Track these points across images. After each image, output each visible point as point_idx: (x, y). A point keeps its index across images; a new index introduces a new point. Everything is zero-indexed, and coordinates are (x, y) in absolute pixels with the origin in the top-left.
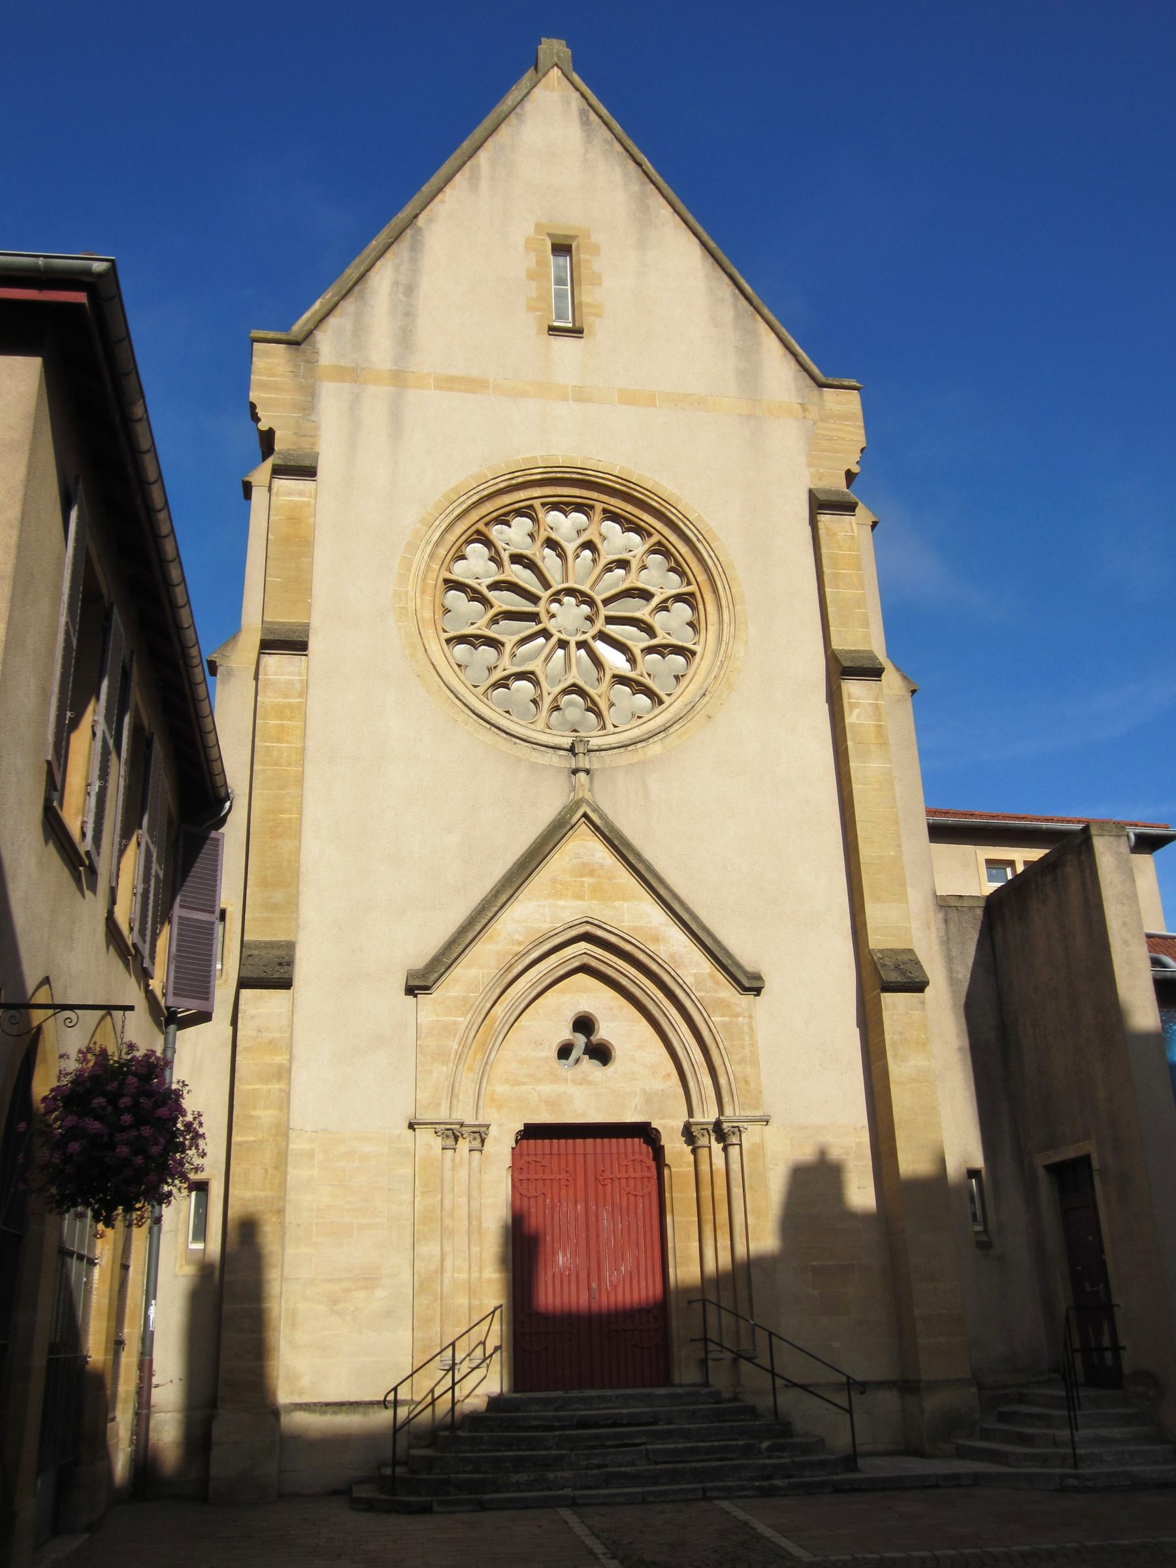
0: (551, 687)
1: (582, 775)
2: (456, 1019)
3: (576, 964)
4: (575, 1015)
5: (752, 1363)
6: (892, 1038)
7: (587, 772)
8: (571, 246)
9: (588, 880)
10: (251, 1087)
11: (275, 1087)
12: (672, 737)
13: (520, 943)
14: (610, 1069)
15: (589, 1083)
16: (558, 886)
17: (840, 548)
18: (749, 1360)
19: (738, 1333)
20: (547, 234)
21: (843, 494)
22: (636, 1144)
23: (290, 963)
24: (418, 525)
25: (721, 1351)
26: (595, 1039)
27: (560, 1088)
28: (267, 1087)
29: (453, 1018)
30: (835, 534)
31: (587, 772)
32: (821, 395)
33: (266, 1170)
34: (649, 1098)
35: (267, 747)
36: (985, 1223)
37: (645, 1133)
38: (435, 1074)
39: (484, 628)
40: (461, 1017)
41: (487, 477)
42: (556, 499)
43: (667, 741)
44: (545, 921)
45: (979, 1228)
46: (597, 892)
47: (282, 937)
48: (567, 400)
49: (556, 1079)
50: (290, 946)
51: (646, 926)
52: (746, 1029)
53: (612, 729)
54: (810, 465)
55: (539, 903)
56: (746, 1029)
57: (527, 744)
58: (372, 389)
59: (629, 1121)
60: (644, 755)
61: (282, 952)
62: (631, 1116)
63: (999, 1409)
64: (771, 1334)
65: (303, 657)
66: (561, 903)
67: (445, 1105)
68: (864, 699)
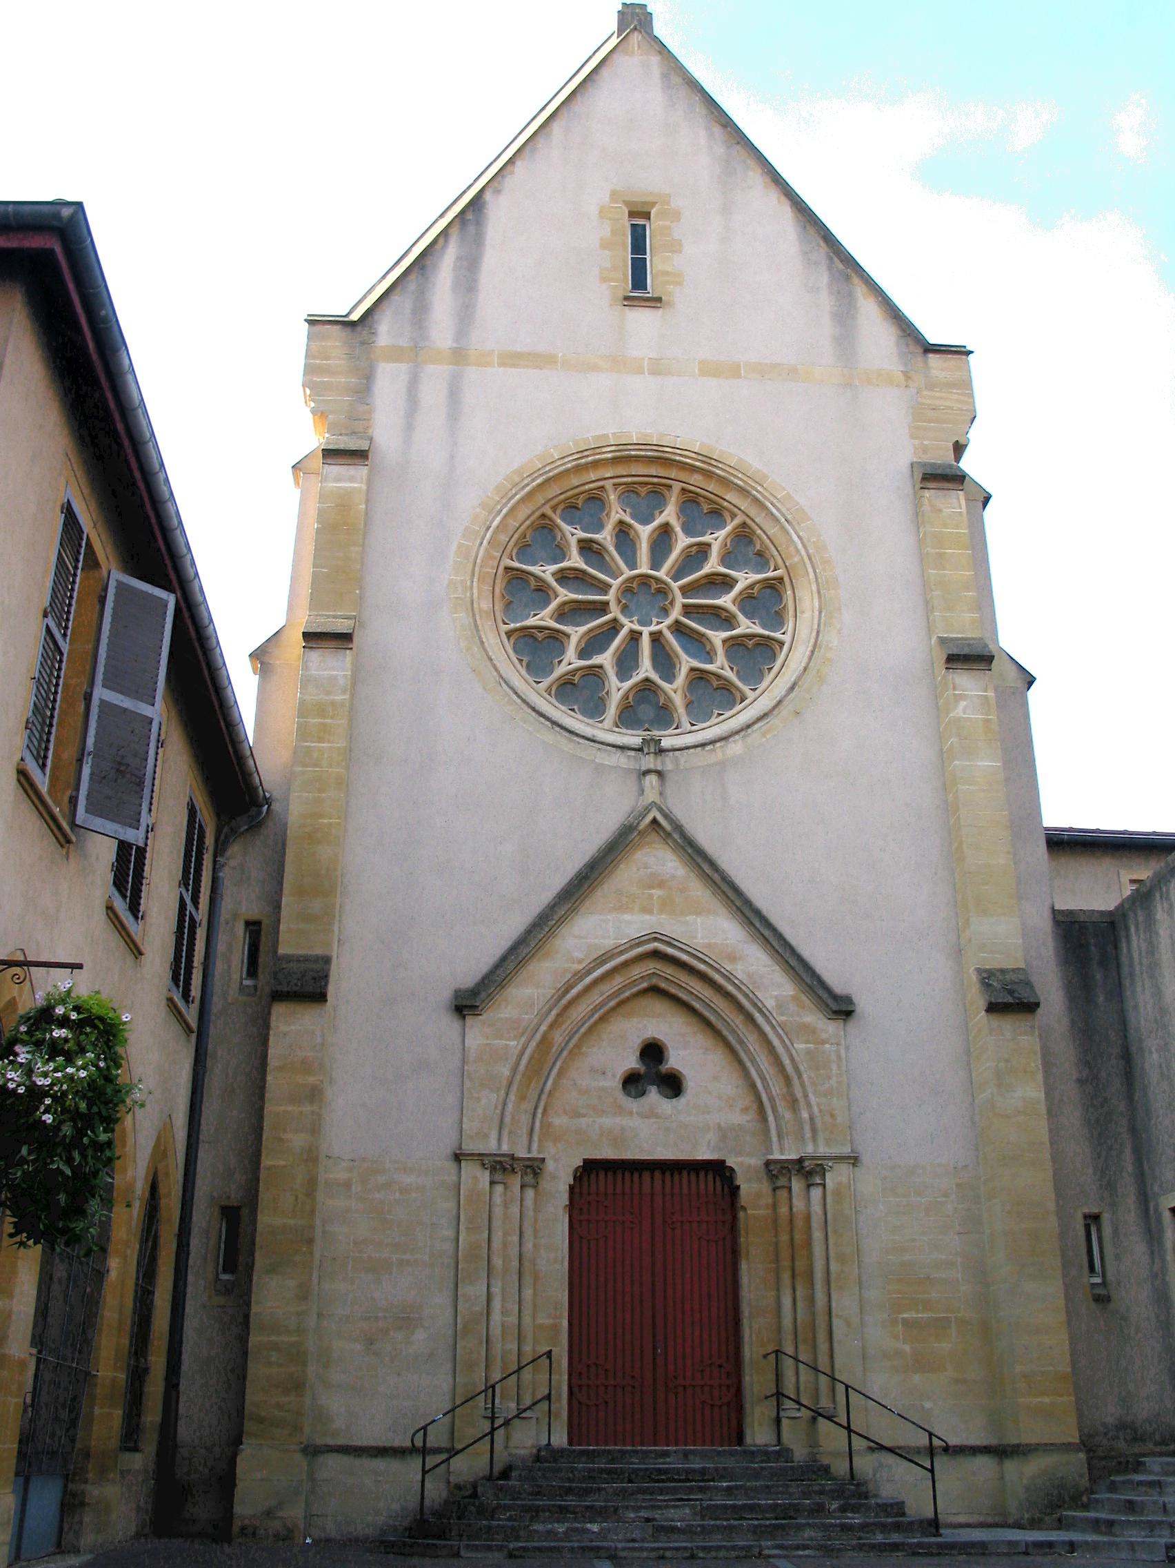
0: (622, 682)
1: (652, 779)
2: (508, 1043)
3: (645, 985)
4: (642, 1042)
5: (832, 1421)
6: (997, 1065)
7: (660, 774)
8: (649, 213)
9: (657, 892)
10: (282, 1108)
11: (307, 1108)
12: (755, 735)
13: (580, 962)
14: (682, 1101)
15: (657, 1116)
16: (624, 899)
17: (945, 526)
18: (830, 1418)
19: (817, 1390)
20: (624, 201)
21: (950, 466)
22: (707, 1183)
23: (326, 977)
24: (478, 510)
25: (799, 1410)
26: (664, 1068)
27: (625, 1121)
28: (300, 1109)
29: (504, 1042)
30: (940, 511)
31: (660, 774)
32: (926, 363)
33: (297, 1197)
34: (724, 1133)
35: (307, 747)
36: (1104, 1276)
37: (718, 1169)
38: (484, 1101)
39: (548, 619)
40: (513, 1040)
41: (553, 457)
42: (629, 479)
43: (749, 740)
44: (609, 937)
45: (1098, 1280)
46: (666, 905)
47: (318, 951)
48: (643, 373)
49: (620, 1110)
50: (327, 960)
51: (722, 944)
52: (833, 1057)
53: (689, 727)
54: (912, 437)
55: (602, 917)
56: (833, 1057)
57: (592, 744)
58: (431, 369)
59: (700, 1158)
60: (723, 754)
61: (317, 966)
62: (704, 1154)
63: (1112, 1478)
64: (847, 1387)
65: (348, 651)
66: (627, 917)
67: (494, 1135)
68: (971, 691)
